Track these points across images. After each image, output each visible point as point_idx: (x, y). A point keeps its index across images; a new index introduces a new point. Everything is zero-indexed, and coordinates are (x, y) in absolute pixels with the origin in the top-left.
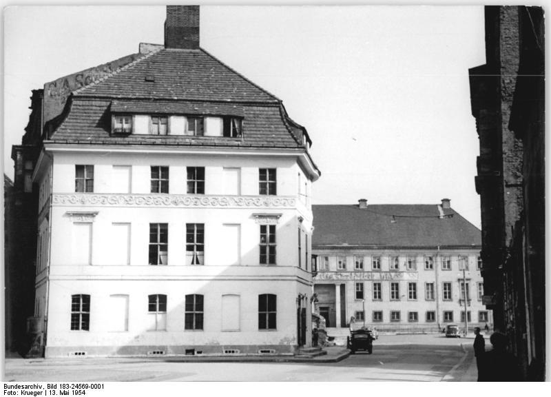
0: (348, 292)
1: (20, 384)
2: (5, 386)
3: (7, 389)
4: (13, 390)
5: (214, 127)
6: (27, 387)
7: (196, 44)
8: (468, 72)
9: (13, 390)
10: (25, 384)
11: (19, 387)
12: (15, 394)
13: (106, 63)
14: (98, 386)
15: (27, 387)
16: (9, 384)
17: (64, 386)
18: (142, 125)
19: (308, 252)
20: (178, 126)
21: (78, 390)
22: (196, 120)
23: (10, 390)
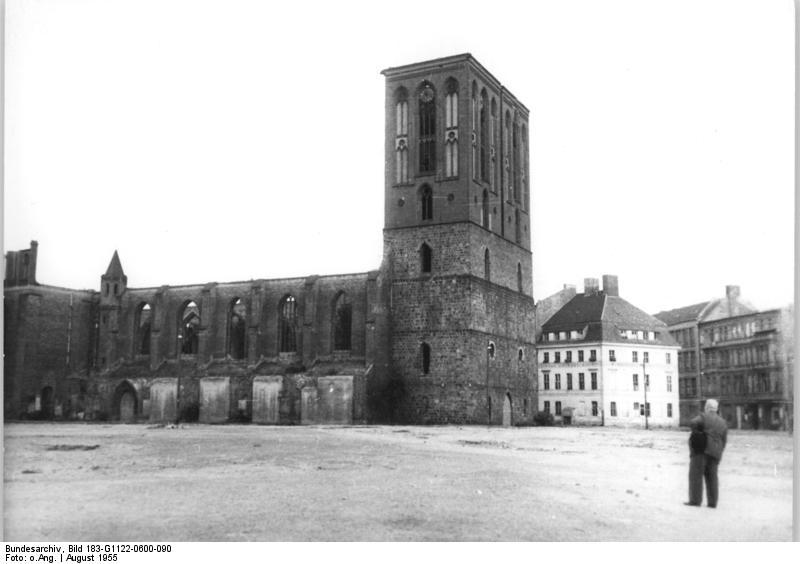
0: (777, 438)
1: (29, 544)
2: (8, 548)
3: (10, 553)
4: (19, 554)
5: (651, 336)
7: (617, 295)
8: (100, 279)
9: (19, 554)
10: (36, 544)
11: (28, 549)
12: (21, 559)
13: (249, 279)
14: (149, 548)
16: (13, 545)
17: (93, 548)
18: (629, 334)
19: (43, 439)
20: (563, 335)
21: (108, 554)
22: (557, 334)
23: (14, 554)
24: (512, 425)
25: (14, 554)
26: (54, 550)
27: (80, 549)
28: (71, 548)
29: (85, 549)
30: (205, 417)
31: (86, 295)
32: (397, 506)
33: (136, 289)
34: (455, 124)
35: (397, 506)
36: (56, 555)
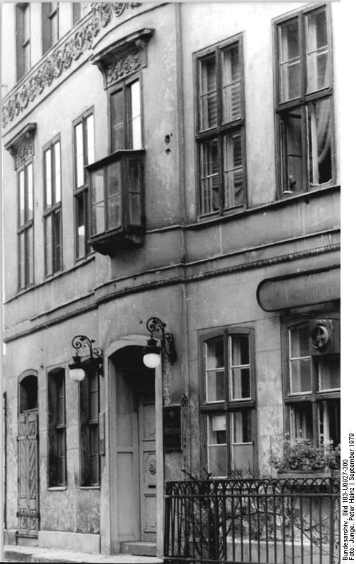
2: (345, 559)
3: (348, 557)
4: (349, 550)
6: (346, 537)
9: (349, 550)
11: (346, 544)
15: (346, 537)
23: (349, 554)
24: (111, 554)
25: (349, 554)
26: (346, 526)
27: (346, 507)
28: (345, 514)
29: (345, 504)
30: (336, 293)
31: (121, 378)
32: (72, 505)
33: (256, 417)
34: (173, 499)
35: (72, 505)
36: (350, 524)
